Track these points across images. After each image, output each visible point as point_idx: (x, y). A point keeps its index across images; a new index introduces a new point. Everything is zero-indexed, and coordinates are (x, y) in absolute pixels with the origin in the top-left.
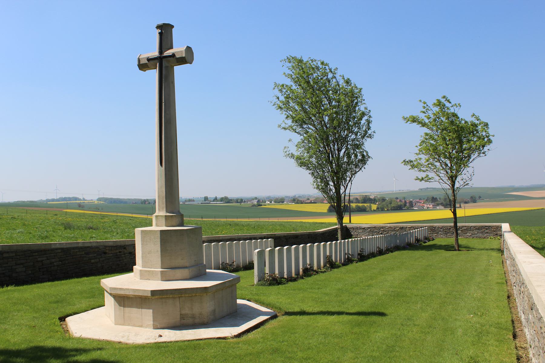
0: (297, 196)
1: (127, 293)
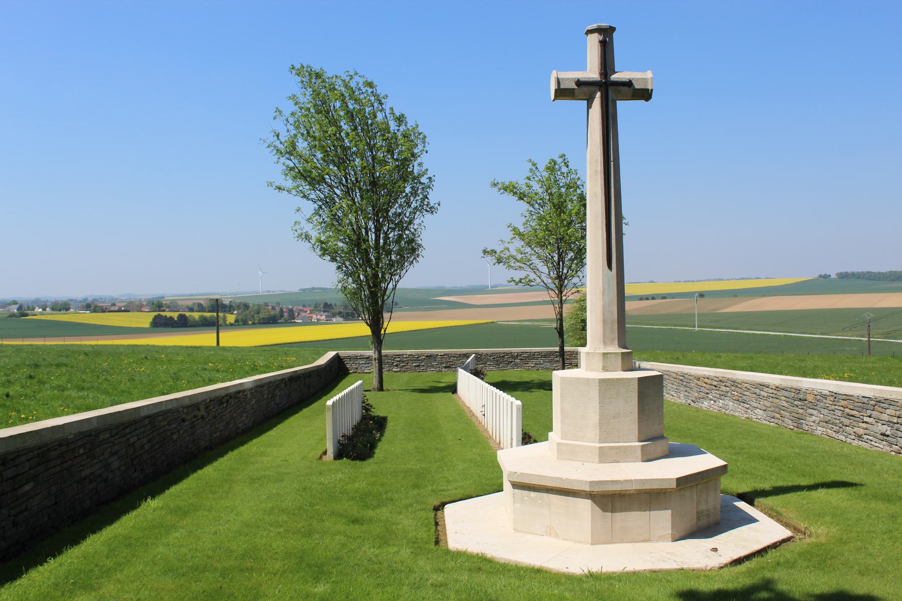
1: (628, 487)
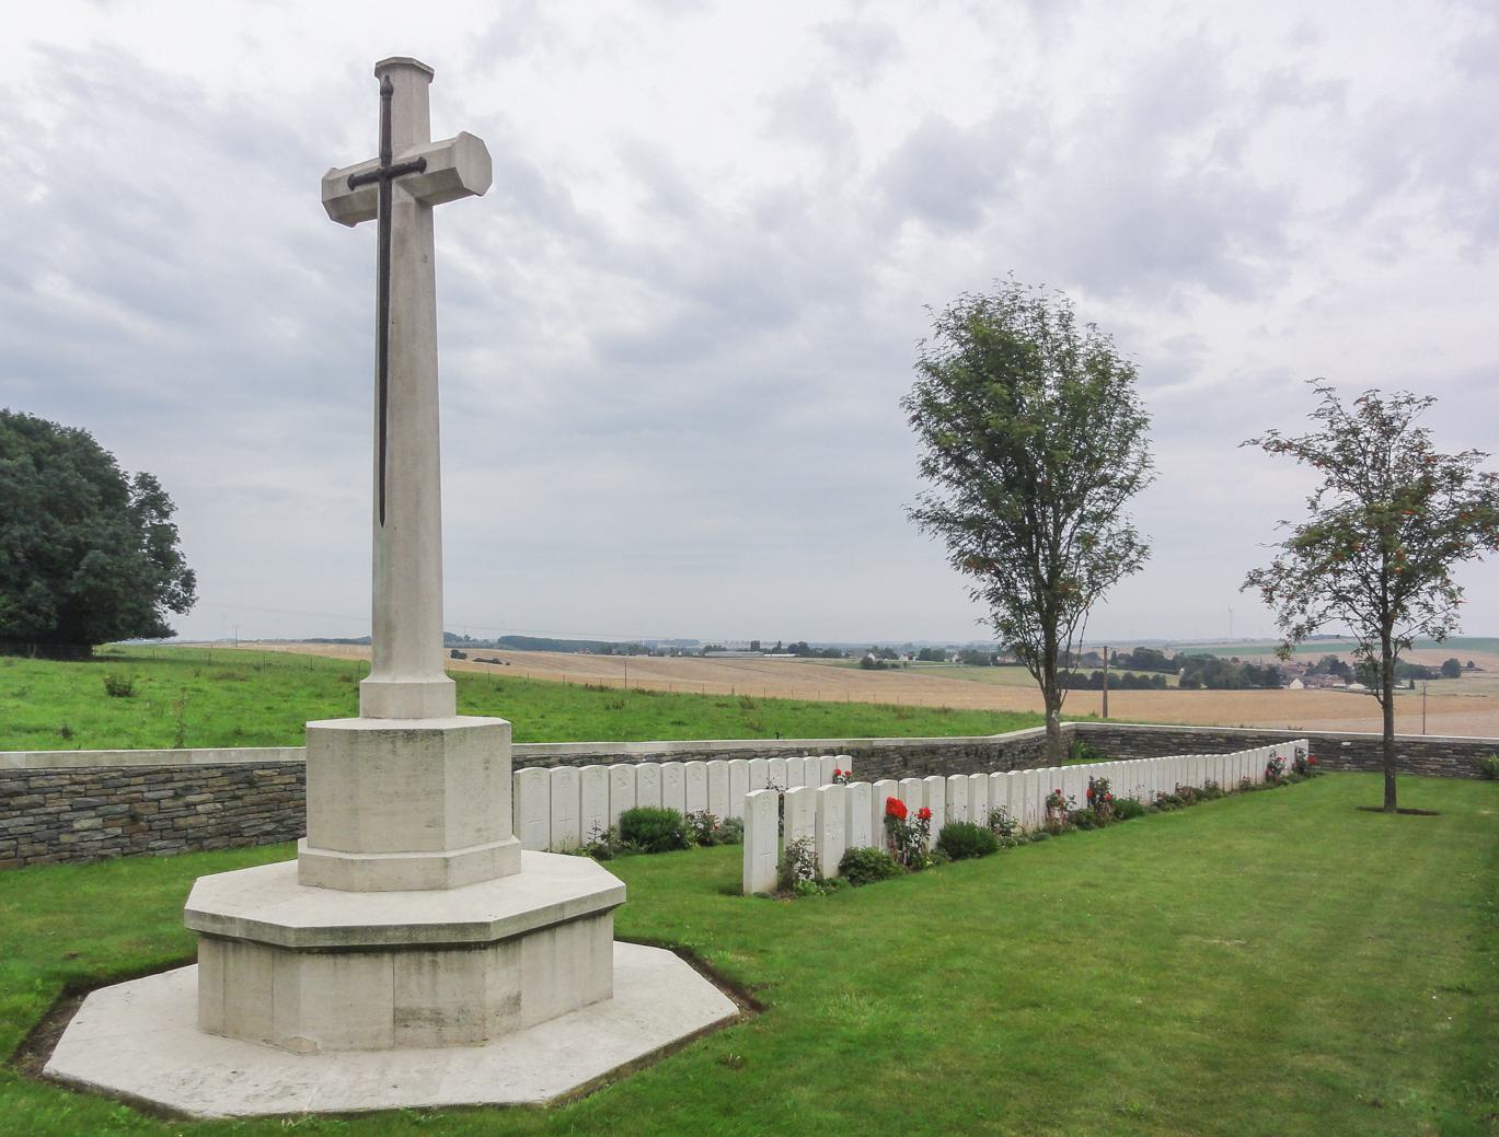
0: (976, 644)
